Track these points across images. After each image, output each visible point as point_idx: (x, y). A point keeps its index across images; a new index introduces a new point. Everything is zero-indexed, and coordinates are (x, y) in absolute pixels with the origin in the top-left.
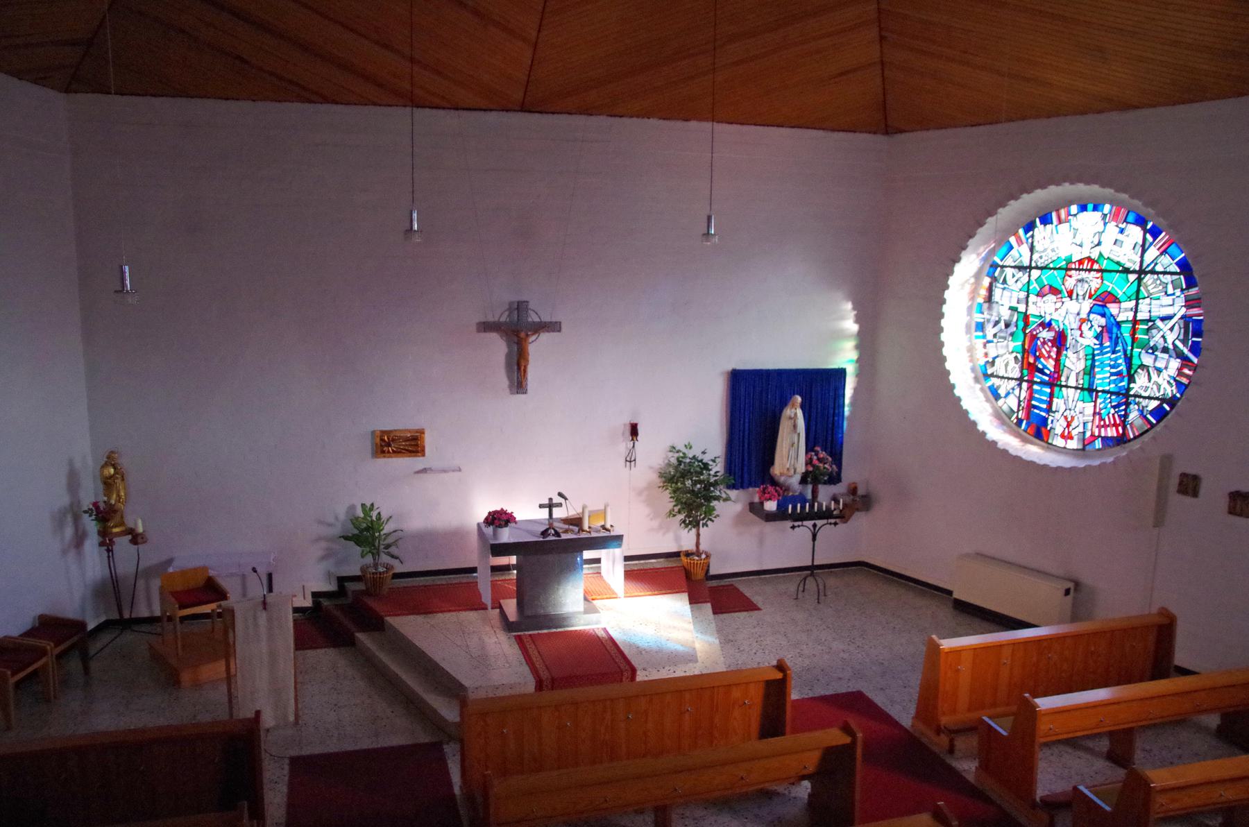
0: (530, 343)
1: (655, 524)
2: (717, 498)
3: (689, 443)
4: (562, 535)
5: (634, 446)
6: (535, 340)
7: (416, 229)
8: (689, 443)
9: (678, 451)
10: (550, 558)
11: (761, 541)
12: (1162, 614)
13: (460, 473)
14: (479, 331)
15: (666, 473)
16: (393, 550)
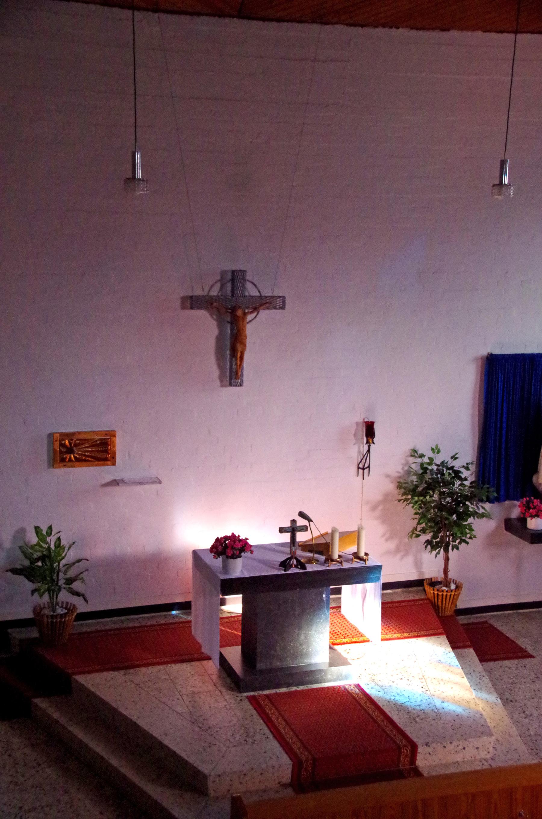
0: (248, 323)
1: (392, 545)
2: (475, 514)
3: (437, 446)
4: (307, 566)
5: (369, 451)
6: (253, 319)
7: (140, 177)
8: (437, 446)
9: (422, 456)
10: (288, 595)
11: (518, 566)
12: (245, 546)
13: (159, 485)
14: (183, 307)
15: (408, 483)
16: (76, 586)
